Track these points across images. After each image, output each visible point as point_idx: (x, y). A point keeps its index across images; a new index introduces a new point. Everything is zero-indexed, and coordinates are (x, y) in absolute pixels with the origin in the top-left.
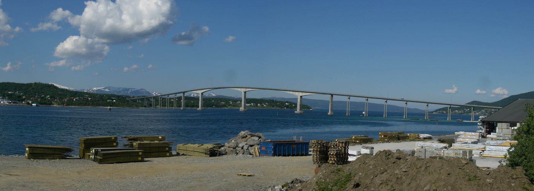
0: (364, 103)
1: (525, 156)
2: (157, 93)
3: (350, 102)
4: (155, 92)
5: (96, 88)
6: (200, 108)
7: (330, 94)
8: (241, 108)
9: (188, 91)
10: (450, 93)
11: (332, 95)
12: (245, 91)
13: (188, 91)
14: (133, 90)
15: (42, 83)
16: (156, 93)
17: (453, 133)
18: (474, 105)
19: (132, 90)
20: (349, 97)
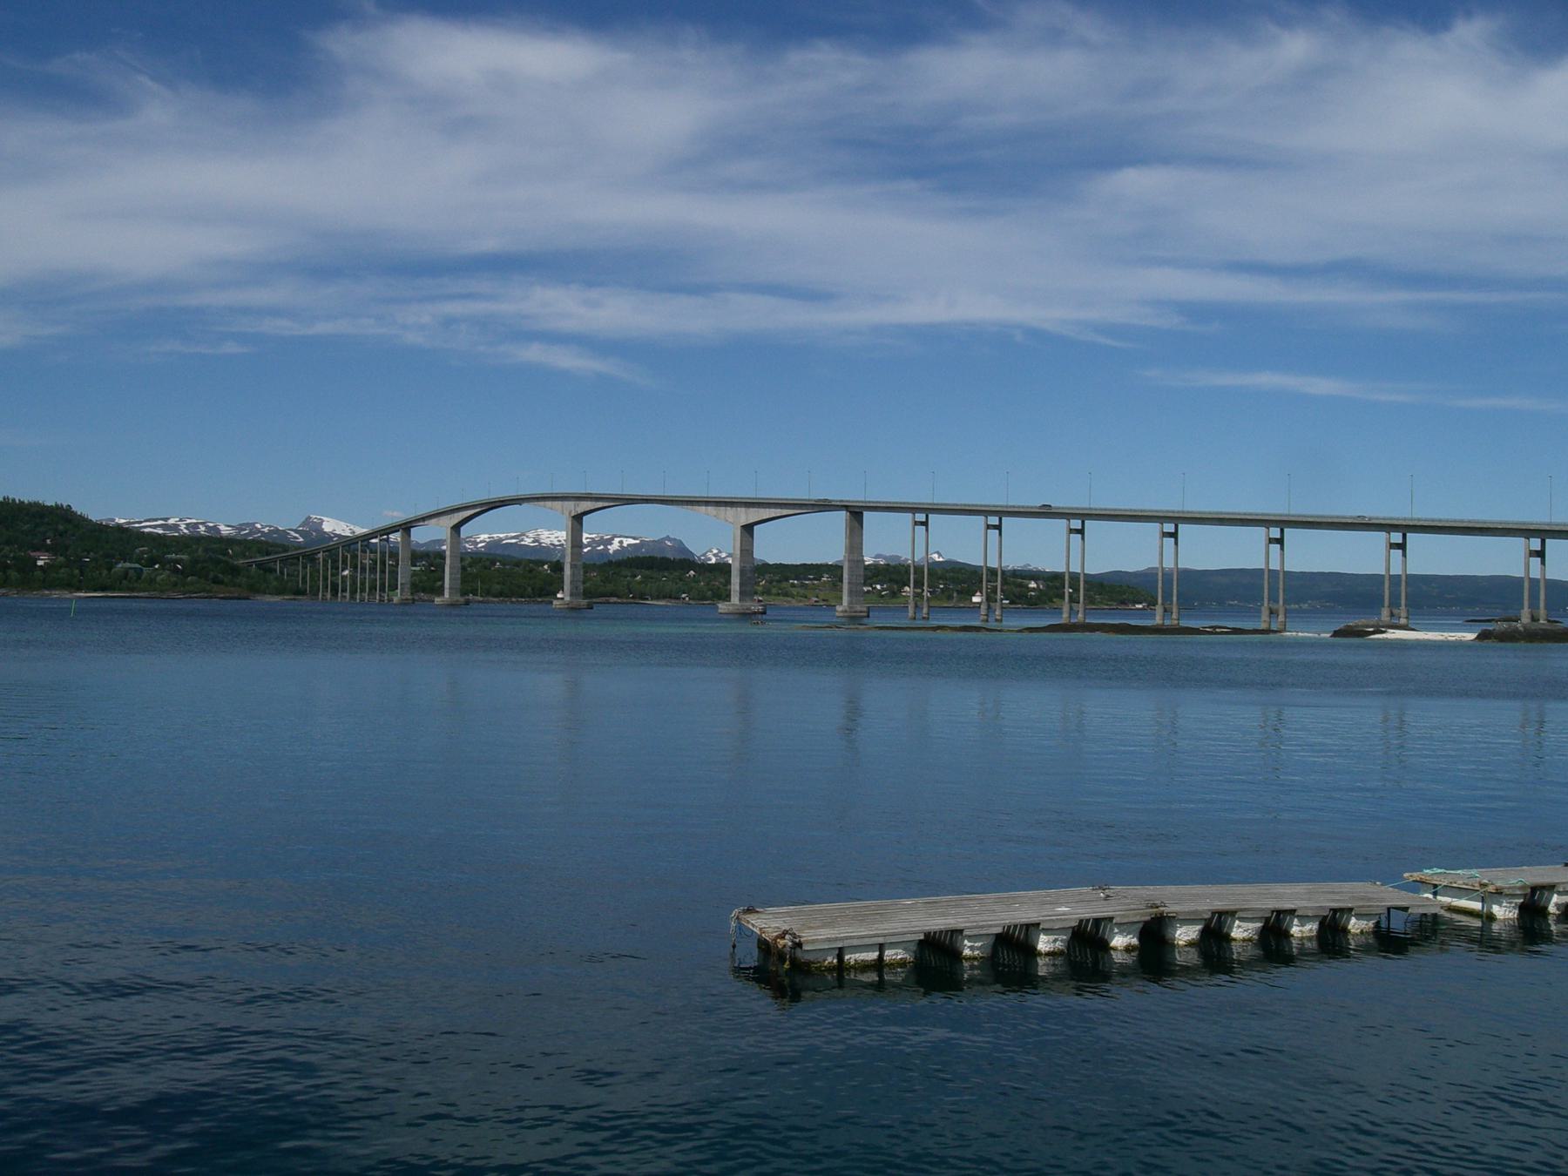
0: (1515, 583)
1: (395, 604)
2: (723, 555)
3: (1413, 580)
4: (715, 551)
5: (486, 536)
6: (735, 599)
7: (846, 508)
8: (559, 596)
9: (424, 519)
10: (783, 906)
11: (856, 514)
12: (573, 514)
13: (424, 519)
14: (625, 545)
15: (22, 503)
16: (720, 552)
17: (1483, 636)
18: (1263, 584)
19: (621, 542)
20: (1535, 544)
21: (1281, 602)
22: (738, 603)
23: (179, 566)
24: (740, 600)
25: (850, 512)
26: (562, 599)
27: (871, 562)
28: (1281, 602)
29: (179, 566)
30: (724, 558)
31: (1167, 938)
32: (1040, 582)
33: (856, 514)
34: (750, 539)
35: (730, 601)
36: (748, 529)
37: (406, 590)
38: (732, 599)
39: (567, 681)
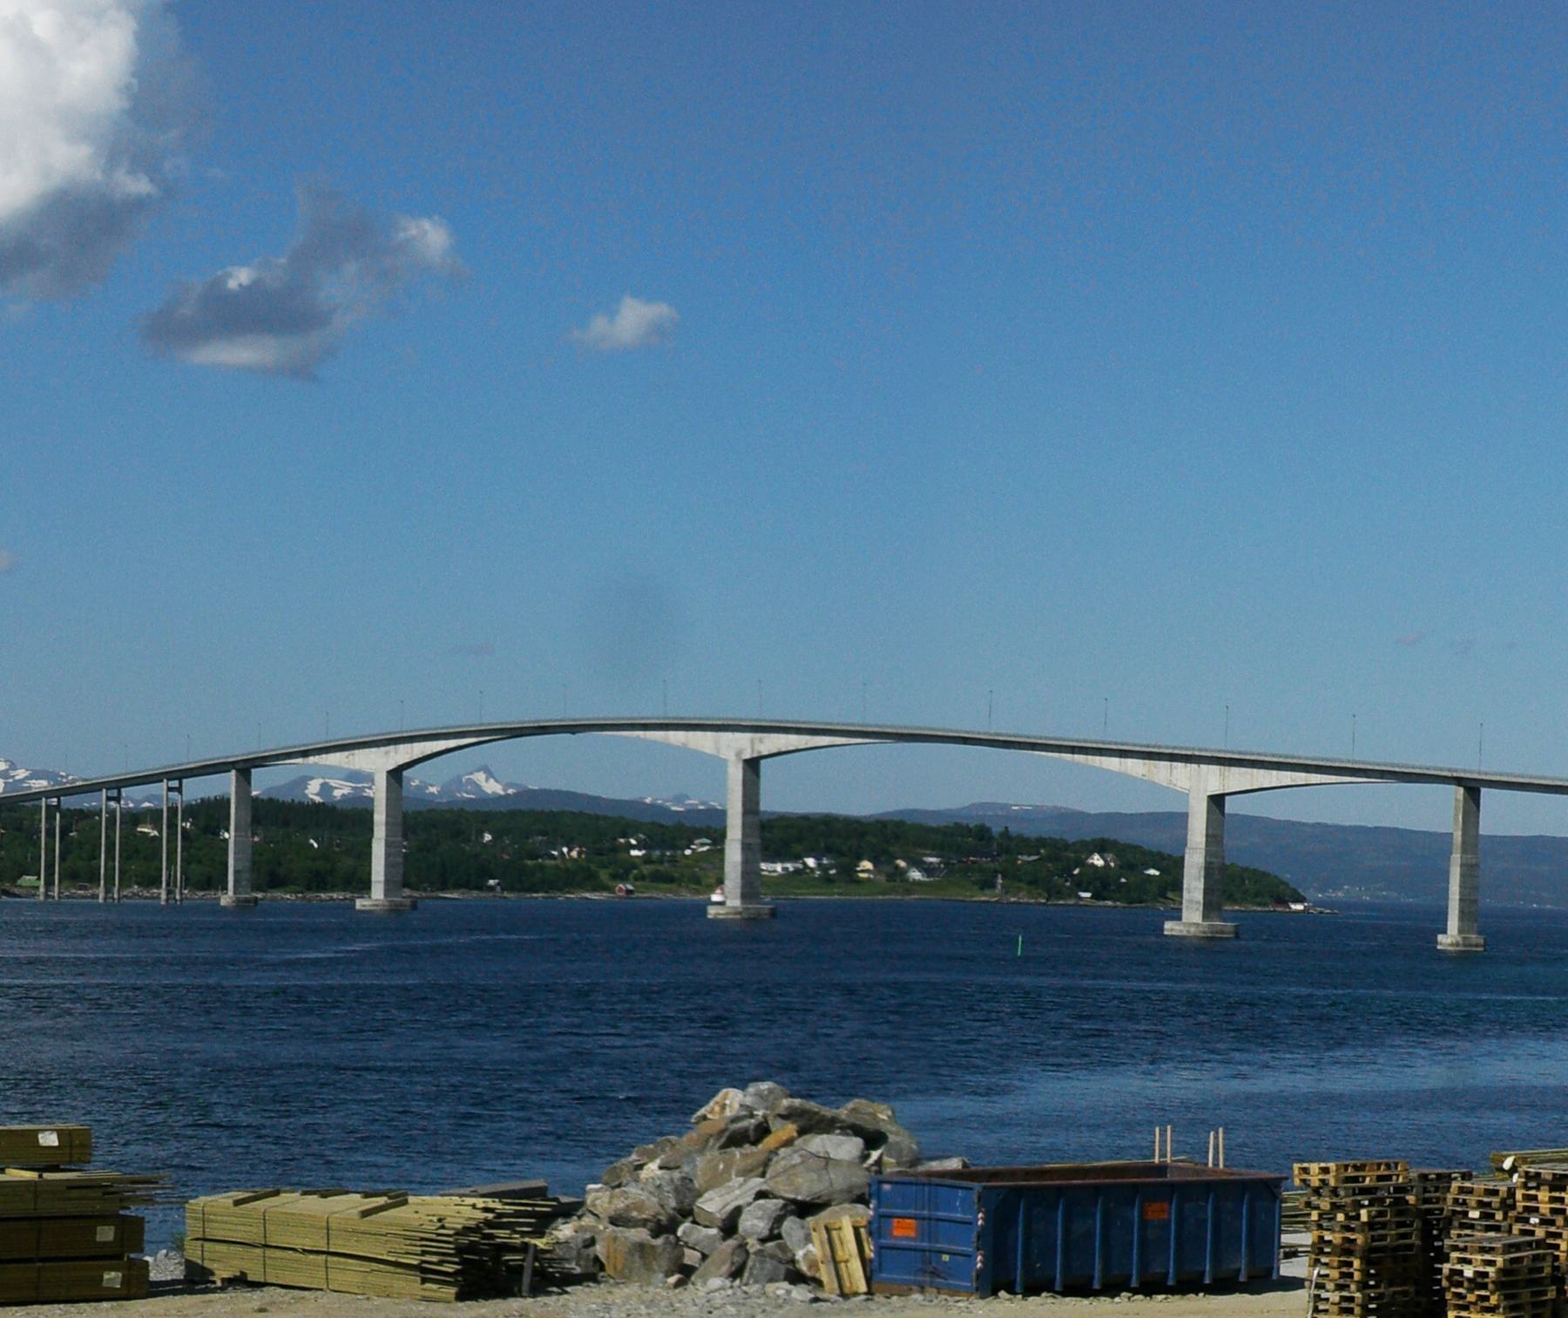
2: (21, 774)
7: (1458, 781)
8: (716, 897)
16: (13, 767)
21: (1169, 1155)
22: (1200, 921)
23: (1152, 872)
24: (1204, 918)
25: (1465, 788)
26: (721, 904)
27: (346, 791)
28: (1169, 1155)
29: (1152, 872)
30: (22, 781)
31: (126, 104)
32: (1110, 857)
33: (1473, 789)
34: (755, 777)
35: (1180, 918)
36: (752, 765)
37: (244, 883)
38: (1185, 914)
39: (1178, 1142)
